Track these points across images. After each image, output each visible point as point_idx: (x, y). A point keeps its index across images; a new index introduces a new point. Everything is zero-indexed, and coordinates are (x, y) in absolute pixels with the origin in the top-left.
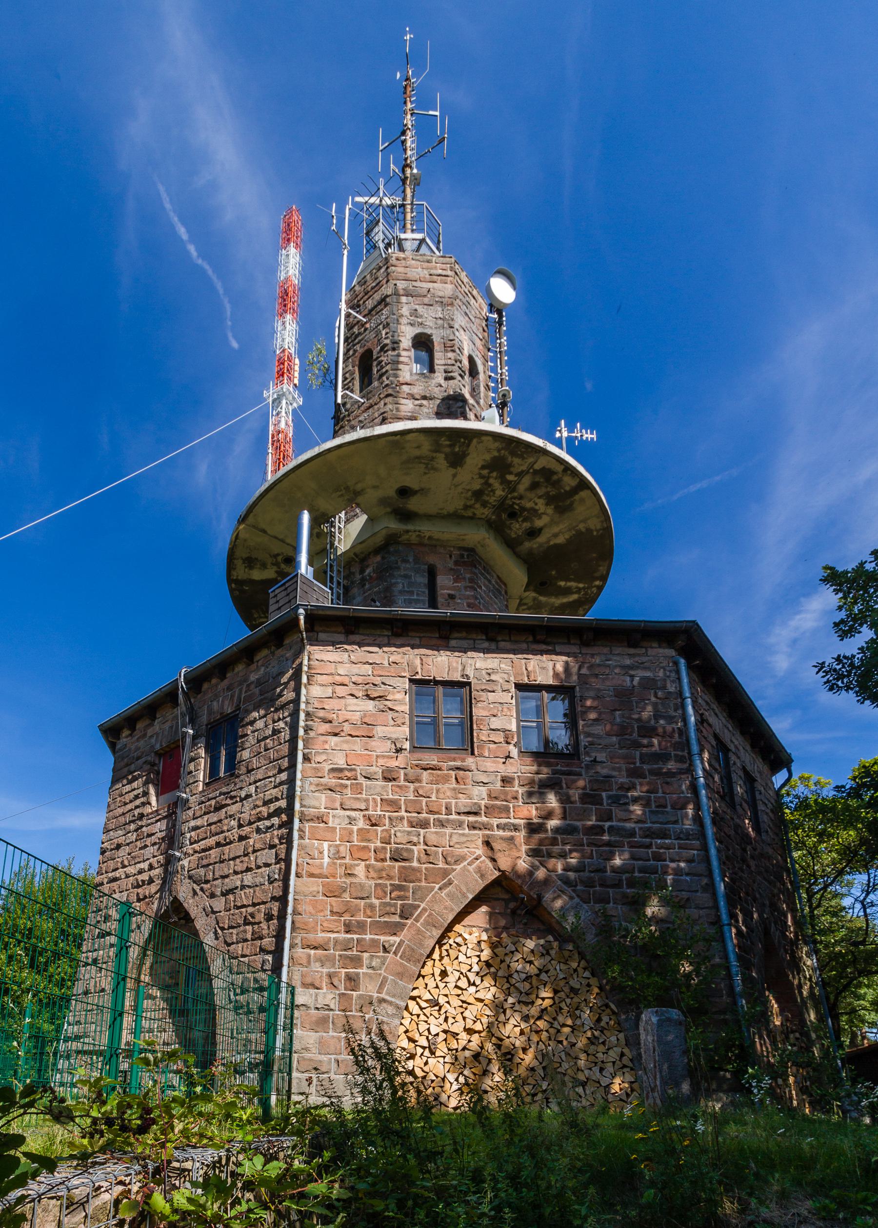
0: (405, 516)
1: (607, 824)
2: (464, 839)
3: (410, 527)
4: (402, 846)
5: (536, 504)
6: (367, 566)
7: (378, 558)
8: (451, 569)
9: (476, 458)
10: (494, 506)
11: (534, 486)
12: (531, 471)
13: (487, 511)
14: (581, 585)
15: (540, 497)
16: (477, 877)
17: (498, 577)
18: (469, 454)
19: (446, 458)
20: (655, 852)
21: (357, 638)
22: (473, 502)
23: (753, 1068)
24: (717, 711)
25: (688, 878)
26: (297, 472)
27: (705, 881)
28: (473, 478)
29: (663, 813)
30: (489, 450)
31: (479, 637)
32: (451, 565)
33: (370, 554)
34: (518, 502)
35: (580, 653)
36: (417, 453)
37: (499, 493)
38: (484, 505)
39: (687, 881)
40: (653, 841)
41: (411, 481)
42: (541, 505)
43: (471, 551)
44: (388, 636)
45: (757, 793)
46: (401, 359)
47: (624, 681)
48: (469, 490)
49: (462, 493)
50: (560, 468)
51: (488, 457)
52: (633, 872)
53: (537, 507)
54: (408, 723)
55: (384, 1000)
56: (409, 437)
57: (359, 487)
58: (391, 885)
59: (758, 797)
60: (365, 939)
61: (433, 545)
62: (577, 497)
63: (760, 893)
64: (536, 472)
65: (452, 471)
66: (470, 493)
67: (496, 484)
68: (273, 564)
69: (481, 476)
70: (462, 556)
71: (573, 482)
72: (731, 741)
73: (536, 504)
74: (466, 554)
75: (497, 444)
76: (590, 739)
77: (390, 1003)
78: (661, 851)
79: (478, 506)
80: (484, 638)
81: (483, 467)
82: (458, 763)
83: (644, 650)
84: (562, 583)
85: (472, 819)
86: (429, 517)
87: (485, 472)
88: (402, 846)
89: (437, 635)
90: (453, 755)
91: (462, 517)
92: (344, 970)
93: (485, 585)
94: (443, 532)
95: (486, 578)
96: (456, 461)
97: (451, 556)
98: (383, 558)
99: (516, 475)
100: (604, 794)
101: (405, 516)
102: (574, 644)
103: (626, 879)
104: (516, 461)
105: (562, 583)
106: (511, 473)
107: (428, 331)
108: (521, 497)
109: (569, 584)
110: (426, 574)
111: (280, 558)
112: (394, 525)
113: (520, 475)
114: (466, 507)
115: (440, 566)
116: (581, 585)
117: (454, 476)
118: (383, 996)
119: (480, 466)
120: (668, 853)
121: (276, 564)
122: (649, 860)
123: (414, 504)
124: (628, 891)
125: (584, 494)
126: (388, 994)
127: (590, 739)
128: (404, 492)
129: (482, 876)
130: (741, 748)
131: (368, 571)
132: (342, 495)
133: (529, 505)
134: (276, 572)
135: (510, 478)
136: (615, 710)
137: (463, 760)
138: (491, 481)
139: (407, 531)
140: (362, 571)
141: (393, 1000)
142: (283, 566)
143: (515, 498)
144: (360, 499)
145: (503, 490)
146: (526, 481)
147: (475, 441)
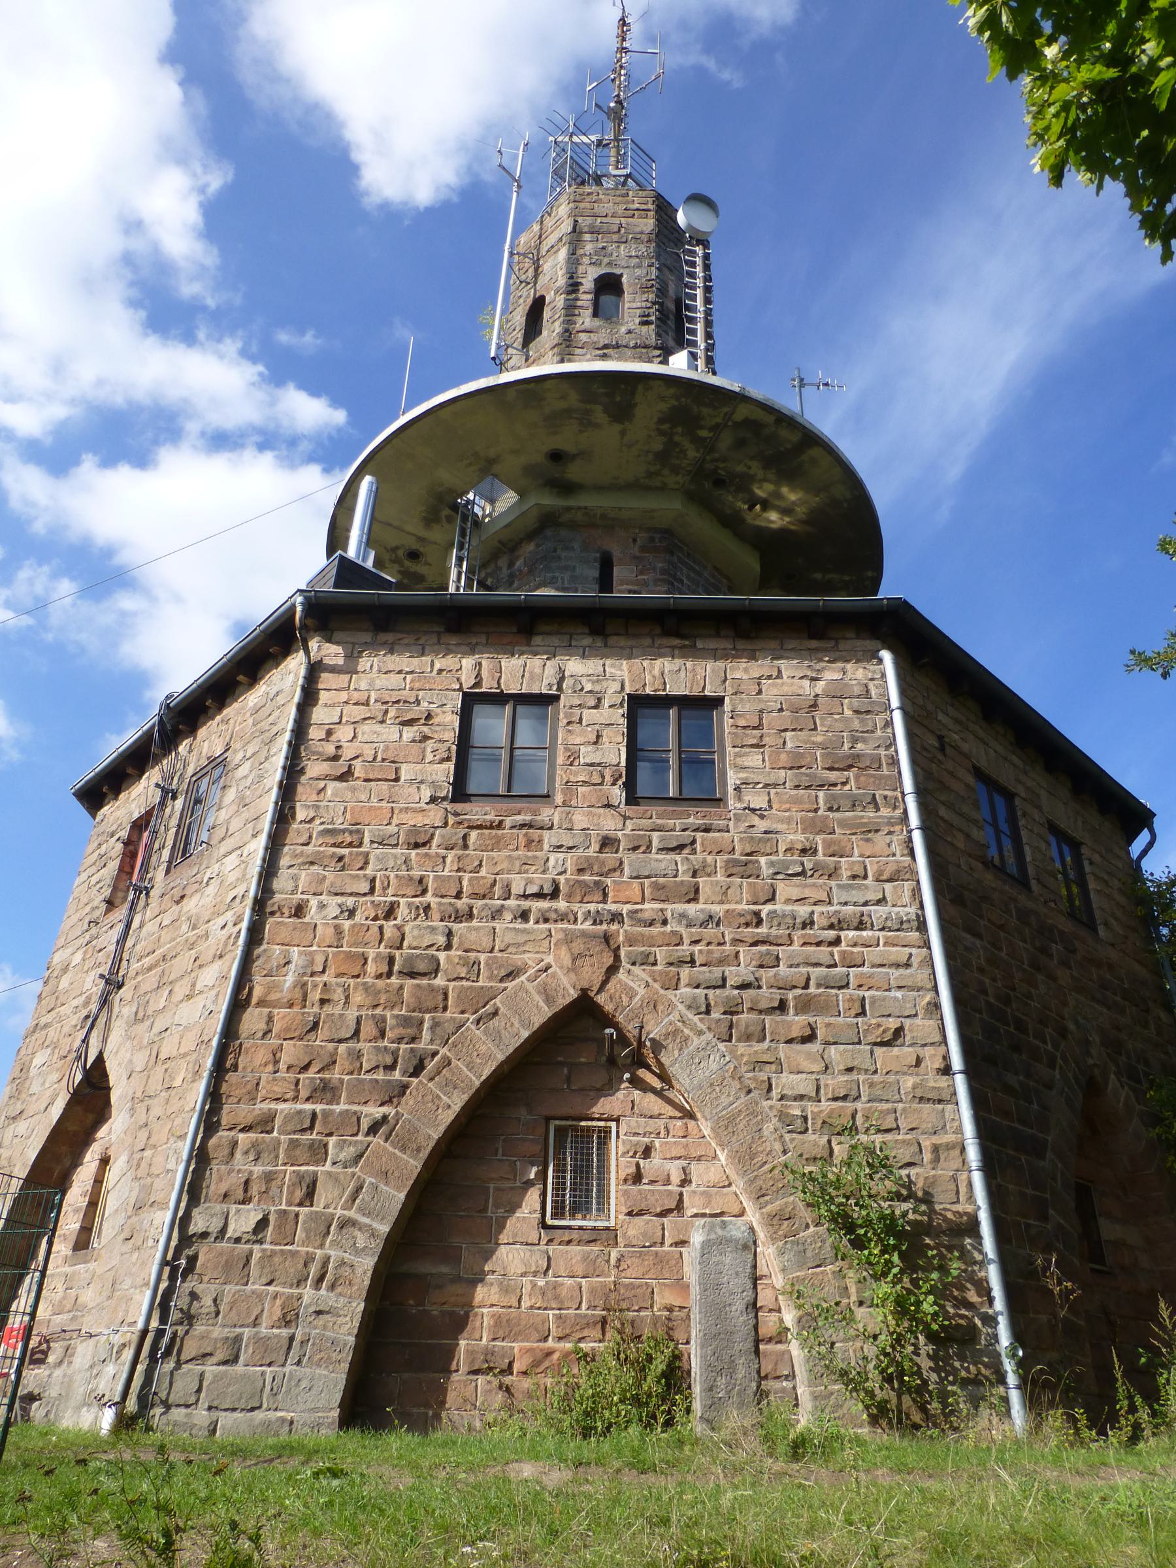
0: (567, 488)
1: (766, 909)
2: (521, 938)
3: (572, 502)
4: (418, 952)
5: (750, 468)
6: (518, 558)
7: (531, 547)
8: (635, 558)
9: (647, 411)
10: (690, 472)
11: (740, 443)
12: (730, 423)
13: (680, 479)
14: (847, 578)
15: (752, 458)
16: (539, 1000)
17: (715, 568)
18: (636, 405)
19: (606, 411)
20: (845, 952)
21: (390, 637)
22: (658, 467)
23: (1141, 1356)
24: (982, 734)
25: (899, 994)
26: (402, 436)
27: (928, 997)
28: (650, 436)
29: (859, 887)
30: (662, 399)
31: (579, 631)
32: (635, 551)
33: (521, 541)
34: (722, 465)
35: (734, 649)
36: (563, 405)
37: (692, 453)
38: (675, 470)
39: (896, 999)
40: (843, 934)
41: (565, 441)
42: (756, 468)
43: (667, 533)
44: (439, 633)
45: (1086, 863)
46: (579, 303)
47: (801, 687)
48: (648, 452)
49: (639, 456)
50: (770, 419)
51: (664, 406)
52: (806, 987)
53: (752, 472)
54: (454, 759)
55: (352, 1223)
56: (548, 384)
57: (492, 453)
58: (393, 1016)
59: (1087, 868)
60: (332, 1111)
61: (609, 523)
62: (805, 457)
63: (1076, 1022)
64: (737, 425)
65: (617, 427)
66: (651, 456)
67: (686, 444)
68: (394, 562)
69: (661, 433)
70: (652, 540)
71: (795, 437)
72: (1018, 781)
73: (750, 468)
74: (657, 536)
75: (672, 391)
76: (743, 775)
77: (361, 1227)
78: (855, 950)
79: (666, 472)
80: (587, 631)
81: (661, 421)
82: (525, 818)
83: (832, 643)
84: (818, 576)
85: (544, 904)
86: (600, 488)
87: (665, 427)
88: (418, 952)
89: (515, 630)
90: (519, 806)
91: (648, 488)
92: (291, 1169)
93: (688, 577)
94: (620, 509)
95: (691, 568)
96: (622, 413)
97: (635, 540)
98: (538, 546)
99: (711, 429)
100: (763, 860)
101: (567, 488)
102: (726, 637)
103: (795, 998)
104: (705, 411)
105: (818, 576)
106: (701, 428)
107: (617, 271)
108: (725, 460)
109: (830, 576)
110: (597, 565)
111: (400, 553)
112: (548, 500)
113: (715, 428)
114: (650, 475)
115: (616, 553)
116: (847, 578)
117: (623, 433)
118: (352, 1214)
119: (655, 419)
120: (871, 955)
121: (396, 561)
122: (835, 966)
123: (574, 472)
124: (796, 1018)
125: (815, 452)
126: (360, 1210)
127: (743, 775)
128: (556, 456)
129: (549, 1000)
130: (1043, 793)
131: (518, 564)
132: (470, 464)
133: (740, 468)
134: (400, 572)
135: (704, 433)
136: (786, 730)
137: (536, 813)
138: (677, 438)
139: (569, 509)
140: (511, 564)
141: (366, 1220)
142: (407, 563)
143: (716, 460)
144: (496, 468)
145: (697, 451)
146: (726, 440)
147: (640, 388)
